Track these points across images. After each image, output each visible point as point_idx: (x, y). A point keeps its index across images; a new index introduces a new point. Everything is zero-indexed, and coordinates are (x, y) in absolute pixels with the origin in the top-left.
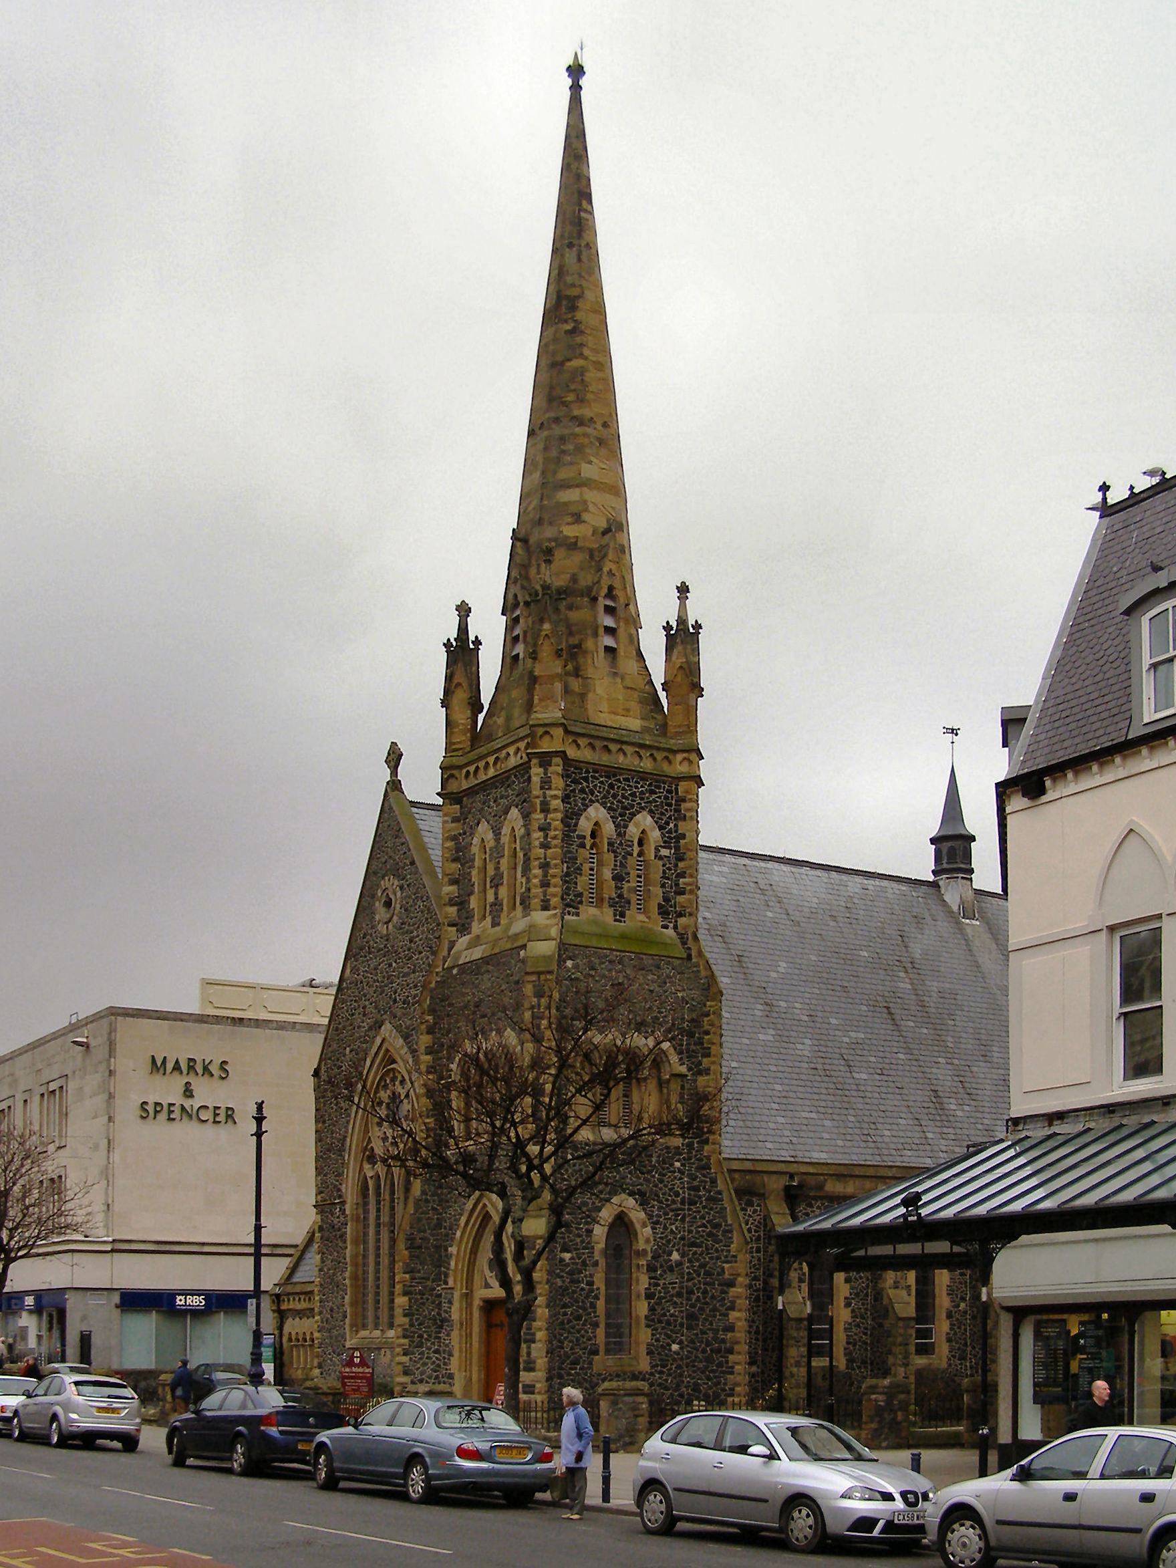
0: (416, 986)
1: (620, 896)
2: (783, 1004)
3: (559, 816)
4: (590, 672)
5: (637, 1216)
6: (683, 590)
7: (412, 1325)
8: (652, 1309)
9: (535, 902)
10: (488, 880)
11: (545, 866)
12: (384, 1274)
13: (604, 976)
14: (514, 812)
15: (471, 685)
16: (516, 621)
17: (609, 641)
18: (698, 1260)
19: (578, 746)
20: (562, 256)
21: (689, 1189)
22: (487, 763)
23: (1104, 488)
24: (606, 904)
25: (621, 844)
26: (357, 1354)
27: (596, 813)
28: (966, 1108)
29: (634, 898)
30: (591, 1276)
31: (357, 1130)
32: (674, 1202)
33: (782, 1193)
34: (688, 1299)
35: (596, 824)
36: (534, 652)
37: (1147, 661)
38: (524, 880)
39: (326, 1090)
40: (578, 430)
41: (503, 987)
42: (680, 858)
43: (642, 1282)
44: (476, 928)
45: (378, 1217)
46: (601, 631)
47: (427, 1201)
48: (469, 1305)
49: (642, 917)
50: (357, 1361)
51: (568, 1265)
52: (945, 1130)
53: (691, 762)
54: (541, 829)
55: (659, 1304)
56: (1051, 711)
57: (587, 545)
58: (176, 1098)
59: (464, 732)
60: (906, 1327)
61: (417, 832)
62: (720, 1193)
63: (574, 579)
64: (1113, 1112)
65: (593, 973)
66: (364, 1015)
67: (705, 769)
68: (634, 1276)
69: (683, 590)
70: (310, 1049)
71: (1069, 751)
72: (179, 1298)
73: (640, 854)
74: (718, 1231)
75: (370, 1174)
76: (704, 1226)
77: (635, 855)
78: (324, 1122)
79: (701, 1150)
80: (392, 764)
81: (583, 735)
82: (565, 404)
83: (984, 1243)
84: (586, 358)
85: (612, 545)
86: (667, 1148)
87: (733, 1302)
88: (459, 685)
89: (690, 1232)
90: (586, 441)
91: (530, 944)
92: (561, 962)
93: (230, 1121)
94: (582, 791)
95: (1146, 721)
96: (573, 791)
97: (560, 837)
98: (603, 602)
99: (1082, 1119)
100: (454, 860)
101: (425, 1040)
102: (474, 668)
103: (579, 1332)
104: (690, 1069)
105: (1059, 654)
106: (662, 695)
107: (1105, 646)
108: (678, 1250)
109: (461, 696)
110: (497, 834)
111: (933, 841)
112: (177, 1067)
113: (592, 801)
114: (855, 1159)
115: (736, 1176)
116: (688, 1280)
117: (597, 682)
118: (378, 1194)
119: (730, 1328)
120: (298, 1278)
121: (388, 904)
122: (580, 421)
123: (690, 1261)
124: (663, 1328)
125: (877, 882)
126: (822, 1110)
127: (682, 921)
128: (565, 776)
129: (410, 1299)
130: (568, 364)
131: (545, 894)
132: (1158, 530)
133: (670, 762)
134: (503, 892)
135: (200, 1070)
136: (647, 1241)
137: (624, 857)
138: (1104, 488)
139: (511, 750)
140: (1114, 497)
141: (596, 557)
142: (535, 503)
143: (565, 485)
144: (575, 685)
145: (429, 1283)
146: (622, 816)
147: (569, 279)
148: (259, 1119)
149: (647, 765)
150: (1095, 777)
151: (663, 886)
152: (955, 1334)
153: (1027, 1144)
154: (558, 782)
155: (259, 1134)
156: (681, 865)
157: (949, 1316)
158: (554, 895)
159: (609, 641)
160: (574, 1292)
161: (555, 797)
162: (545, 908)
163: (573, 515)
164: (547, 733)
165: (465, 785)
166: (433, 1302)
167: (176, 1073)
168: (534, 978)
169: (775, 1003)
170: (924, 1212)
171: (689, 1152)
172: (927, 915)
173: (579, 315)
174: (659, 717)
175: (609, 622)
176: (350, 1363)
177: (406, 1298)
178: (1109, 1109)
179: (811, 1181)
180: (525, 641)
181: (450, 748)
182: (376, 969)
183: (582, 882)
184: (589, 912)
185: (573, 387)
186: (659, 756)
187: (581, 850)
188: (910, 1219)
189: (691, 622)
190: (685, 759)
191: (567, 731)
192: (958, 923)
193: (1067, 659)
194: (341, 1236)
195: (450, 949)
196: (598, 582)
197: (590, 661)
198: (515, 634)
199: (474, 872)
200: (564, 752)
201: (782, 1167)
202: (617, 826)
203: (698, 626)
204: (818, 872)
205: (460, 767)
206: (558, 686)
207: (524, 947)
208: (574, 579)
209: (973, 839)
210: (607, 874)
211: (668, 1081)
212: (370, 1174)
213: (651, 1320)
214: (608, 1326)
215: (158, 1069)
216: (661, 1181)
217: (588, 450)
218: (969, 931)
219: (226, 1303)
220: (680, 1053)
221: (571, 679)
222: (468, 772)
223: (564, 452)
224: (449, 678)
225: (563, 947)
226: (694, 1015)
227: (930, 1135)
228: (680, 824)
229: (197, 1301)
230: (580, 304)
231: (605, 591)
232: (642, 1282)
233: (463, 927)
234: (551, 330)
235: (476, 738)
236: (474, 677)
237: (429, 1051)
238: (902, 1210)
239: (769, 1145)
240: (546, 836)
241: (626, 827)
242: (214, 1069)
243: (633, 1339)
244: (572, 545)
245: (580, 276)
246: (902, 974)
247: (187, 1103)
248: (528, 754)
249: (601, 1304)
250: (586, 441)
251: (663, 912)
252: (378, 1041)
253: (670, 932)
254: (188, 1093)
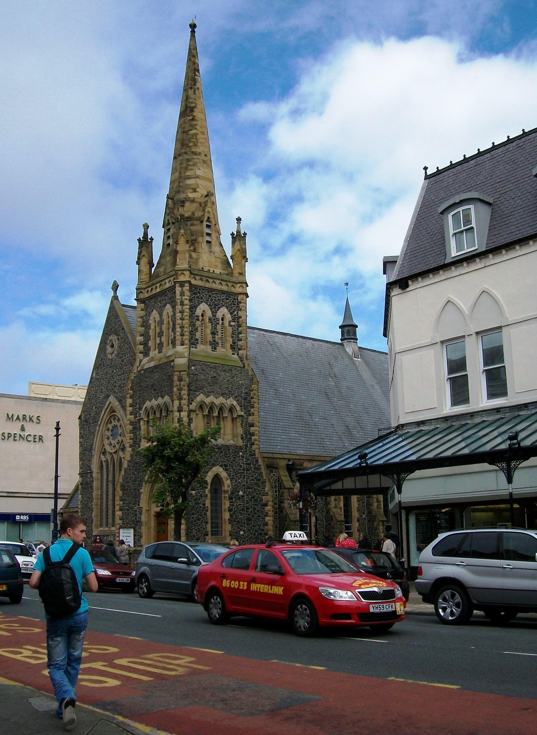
0: (124, 380)
1: (214, 341)
2: (281, 390)
3: (188, 307)
4: (200, 250)
5: (224, 475)
6: (239, 220)
7: (123, 524)
8: (231, 516)
9: (178, 342)
10: (157, 334)
11: (182, 327)
12: (110, 503)
13: (208, 374)
14: (168, 306)
15: (149, 256)
16: (169, 230)
17: (208, 238)
18: (251, 495)
19: (196, 279)
20: (188, 92)
21: (246, 464)
22: (156, 287)
23: (426, 168)
24: (208, 344)
25: (214, 319)
26: (98, 537)
27: (203, 307)
28: (361, 434)
29: (220, 342)
30: (204, 501)
31: (98, 440)
32: (240, 470)
33: (285, 467)
34: (247, 512)
35: (204, 311)
36: (177, 241)
37: (452, 232)
38: (173, 334)
39: (84, 425)
40: (194, 157)
41: (164, 378)
42: (240, 326)
43: (226, 504)
44: (152, 354)
45: (107, 478)
46: (205, 234)
47: (130, 470)
48: (149, 515)
49: (223, 350)
50: (98, 540)
51: (194, 496)
52: (353, 442)
53: (243, 287)
54: (180, 312)
55: (234, 514)
56: (409, 254)
57: (199, 200)
58: (18, 432)
59: (147, 274)
60: (341, 525)
61: (126, 317)
62: (260, 466)
63: (193, 214)
64: (447, 420)
65: (203, 372)
66: (101, 392)
67: (249, 290)
68: (223, 502)
69: (239, 220)
70: (78, 411)
71: (419, 269)
72: (17, 516)
73: (223, 324)
74: (260, 482)
75: (104, 459)
76: (253, 480)
77: (220, 324)
78: (83, 438)
79: (251, 447)
80: (115, 289)
81: (198, 275)
82: (189, 147)
83: (398, 475)
84: (198, 130)
85: (209, 201)
86: (237, 446)
87: (267, 513)
88: (144, 256)
89: (247, 483)
90: (198, 161)
91: (176, 360)
92: (189, 367)
93: (41, 441)
94: (198, 297)
95: (453, 256)
96: (194, 297)
97: (188, 315)
98: (205, 223)
99: (433, 424)
100: (142, 326)
101: (129, 401)
102: (150, 249)
103: (199, 525)
104: (245, 413)
105: (411, 232)
106: (230, 261)
107: (431, 228)
108: (242, 490)
109: (144, 260)
110: (161, 315)
111: (340, 327)
112: (18, 418)
113: (202, 302)
114: (315, 453)
115: (266, 459)
116: (247, 504)
117: (203, 255)
118: (107, 468)
119: (266, 524)
120: (71, 505)
121: (112, 346)
122: (195, 153)
123: (247, 495)
124: (236, 524)
125: (318, 342)
126: (300, 433)
127: (240, 352)
128: (190, 291)
129: (123, 513)
130: (190, 132)
131: (182, 339)
132: (451, 183)
133: (234, 287)
134: (164, 339)
135: (28, 419)
136: (229, 486)
137: (216, 325)
138: (426, 168)
139: (167, 281)
140: (429, 172)
141: (203, 206)
142: (176, 184)
143: (189, 178)
144: (194, 255)
145: (131, 505)
146: (215, 308)
147: (190, 101)
148: (58, 429)
149: (225, 288)
150: (432, 279)
151: (232, 337)
152: (361, 528)
153: (408, 435)
154: (187, 293)
155: (57, 436)
156: (240, 329)
157: (358, 520)
158: (186, 339)
159: (208, 238)
160: (197, 508)
161: (186, 299)
162: (182, 344)
163: (193, 189)
164: (182, 273)
165: (147, 295)
166: (133, 514)
167: (18, 421)
168: (178, 373)
169: (279, 389)
170: (369, 462)
171: (246, 448)
172: (340, 357)
173: (194, 114)
174: (230, 270)
175: (208, 231)
176: (95, 542)
177: (121, 512)
178: (446, 419)
179: (298, 462)
180: (172, 238)
181: (140, 281)
182: (107, 373)
183: (198, 335)
184: (200, 347)
185: (192, 140)
186: (230, 284)
187: (197, 322)
188: (363, 465)
189: (242, 232)
190: (241, 286)
191: (191, 273)
192: (352, 359)
193: (415, 234)
194: (91, 487)
195: (140, 363)
196: (203, 215)
197: (200, 246)
198: (168, 235)
199: (151, 331)
200: (190, 281)
201: (285, 456)
202: (213, 312)
203: (245, 234)
204: (294, 338)
205: (145, 288)
206: (187, 255)
207: (173, 361)
208: (193, 214)
209: (357, 326)
210: (209, 331)
211: (236, 418)
212: (104, 459)
213: (230, 521)
214: (212, 523)
215: (10, 419)
216: (234, 461)
217: (199, 165)
218: (357, 363)
219: (37, 519)
220: (241, 406)
221: (192, 253)
222: (148, 291)
223: (189, 165)
224: (140, 253)
225: (189, 360)
226: (247, 391)
227: (346, 444)
228: (239, 312)
229: (25, 518)
230: (195, 110)
231: (206, 219)
232: (226, 504)
233: (146, 353)
234: (183, 119)
235: (151, 276)
236: (150, 253)
237: (131, 406)
238: (359, 461)
239: (279, 447)
240: (182, 315)
241: (216, 313)
242: (34, 419)
243: (223, 529)
244: (193, 201)
245: (195, 99)
246: (331, 379)
247: (22, 434)
248: (174, 282)
249: (209, 513)
250: (198, 161)
251: (232, 348)
252: (108, 403)
253: (236, 356)
254: (23, 429)
